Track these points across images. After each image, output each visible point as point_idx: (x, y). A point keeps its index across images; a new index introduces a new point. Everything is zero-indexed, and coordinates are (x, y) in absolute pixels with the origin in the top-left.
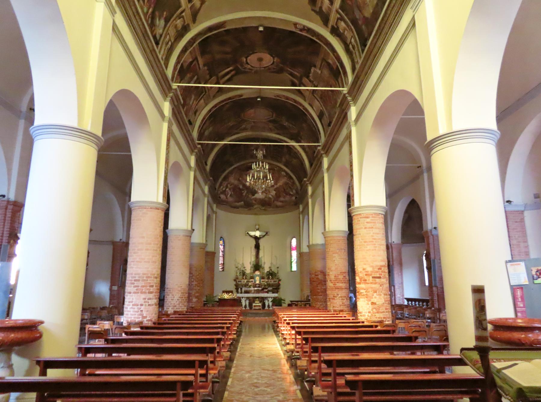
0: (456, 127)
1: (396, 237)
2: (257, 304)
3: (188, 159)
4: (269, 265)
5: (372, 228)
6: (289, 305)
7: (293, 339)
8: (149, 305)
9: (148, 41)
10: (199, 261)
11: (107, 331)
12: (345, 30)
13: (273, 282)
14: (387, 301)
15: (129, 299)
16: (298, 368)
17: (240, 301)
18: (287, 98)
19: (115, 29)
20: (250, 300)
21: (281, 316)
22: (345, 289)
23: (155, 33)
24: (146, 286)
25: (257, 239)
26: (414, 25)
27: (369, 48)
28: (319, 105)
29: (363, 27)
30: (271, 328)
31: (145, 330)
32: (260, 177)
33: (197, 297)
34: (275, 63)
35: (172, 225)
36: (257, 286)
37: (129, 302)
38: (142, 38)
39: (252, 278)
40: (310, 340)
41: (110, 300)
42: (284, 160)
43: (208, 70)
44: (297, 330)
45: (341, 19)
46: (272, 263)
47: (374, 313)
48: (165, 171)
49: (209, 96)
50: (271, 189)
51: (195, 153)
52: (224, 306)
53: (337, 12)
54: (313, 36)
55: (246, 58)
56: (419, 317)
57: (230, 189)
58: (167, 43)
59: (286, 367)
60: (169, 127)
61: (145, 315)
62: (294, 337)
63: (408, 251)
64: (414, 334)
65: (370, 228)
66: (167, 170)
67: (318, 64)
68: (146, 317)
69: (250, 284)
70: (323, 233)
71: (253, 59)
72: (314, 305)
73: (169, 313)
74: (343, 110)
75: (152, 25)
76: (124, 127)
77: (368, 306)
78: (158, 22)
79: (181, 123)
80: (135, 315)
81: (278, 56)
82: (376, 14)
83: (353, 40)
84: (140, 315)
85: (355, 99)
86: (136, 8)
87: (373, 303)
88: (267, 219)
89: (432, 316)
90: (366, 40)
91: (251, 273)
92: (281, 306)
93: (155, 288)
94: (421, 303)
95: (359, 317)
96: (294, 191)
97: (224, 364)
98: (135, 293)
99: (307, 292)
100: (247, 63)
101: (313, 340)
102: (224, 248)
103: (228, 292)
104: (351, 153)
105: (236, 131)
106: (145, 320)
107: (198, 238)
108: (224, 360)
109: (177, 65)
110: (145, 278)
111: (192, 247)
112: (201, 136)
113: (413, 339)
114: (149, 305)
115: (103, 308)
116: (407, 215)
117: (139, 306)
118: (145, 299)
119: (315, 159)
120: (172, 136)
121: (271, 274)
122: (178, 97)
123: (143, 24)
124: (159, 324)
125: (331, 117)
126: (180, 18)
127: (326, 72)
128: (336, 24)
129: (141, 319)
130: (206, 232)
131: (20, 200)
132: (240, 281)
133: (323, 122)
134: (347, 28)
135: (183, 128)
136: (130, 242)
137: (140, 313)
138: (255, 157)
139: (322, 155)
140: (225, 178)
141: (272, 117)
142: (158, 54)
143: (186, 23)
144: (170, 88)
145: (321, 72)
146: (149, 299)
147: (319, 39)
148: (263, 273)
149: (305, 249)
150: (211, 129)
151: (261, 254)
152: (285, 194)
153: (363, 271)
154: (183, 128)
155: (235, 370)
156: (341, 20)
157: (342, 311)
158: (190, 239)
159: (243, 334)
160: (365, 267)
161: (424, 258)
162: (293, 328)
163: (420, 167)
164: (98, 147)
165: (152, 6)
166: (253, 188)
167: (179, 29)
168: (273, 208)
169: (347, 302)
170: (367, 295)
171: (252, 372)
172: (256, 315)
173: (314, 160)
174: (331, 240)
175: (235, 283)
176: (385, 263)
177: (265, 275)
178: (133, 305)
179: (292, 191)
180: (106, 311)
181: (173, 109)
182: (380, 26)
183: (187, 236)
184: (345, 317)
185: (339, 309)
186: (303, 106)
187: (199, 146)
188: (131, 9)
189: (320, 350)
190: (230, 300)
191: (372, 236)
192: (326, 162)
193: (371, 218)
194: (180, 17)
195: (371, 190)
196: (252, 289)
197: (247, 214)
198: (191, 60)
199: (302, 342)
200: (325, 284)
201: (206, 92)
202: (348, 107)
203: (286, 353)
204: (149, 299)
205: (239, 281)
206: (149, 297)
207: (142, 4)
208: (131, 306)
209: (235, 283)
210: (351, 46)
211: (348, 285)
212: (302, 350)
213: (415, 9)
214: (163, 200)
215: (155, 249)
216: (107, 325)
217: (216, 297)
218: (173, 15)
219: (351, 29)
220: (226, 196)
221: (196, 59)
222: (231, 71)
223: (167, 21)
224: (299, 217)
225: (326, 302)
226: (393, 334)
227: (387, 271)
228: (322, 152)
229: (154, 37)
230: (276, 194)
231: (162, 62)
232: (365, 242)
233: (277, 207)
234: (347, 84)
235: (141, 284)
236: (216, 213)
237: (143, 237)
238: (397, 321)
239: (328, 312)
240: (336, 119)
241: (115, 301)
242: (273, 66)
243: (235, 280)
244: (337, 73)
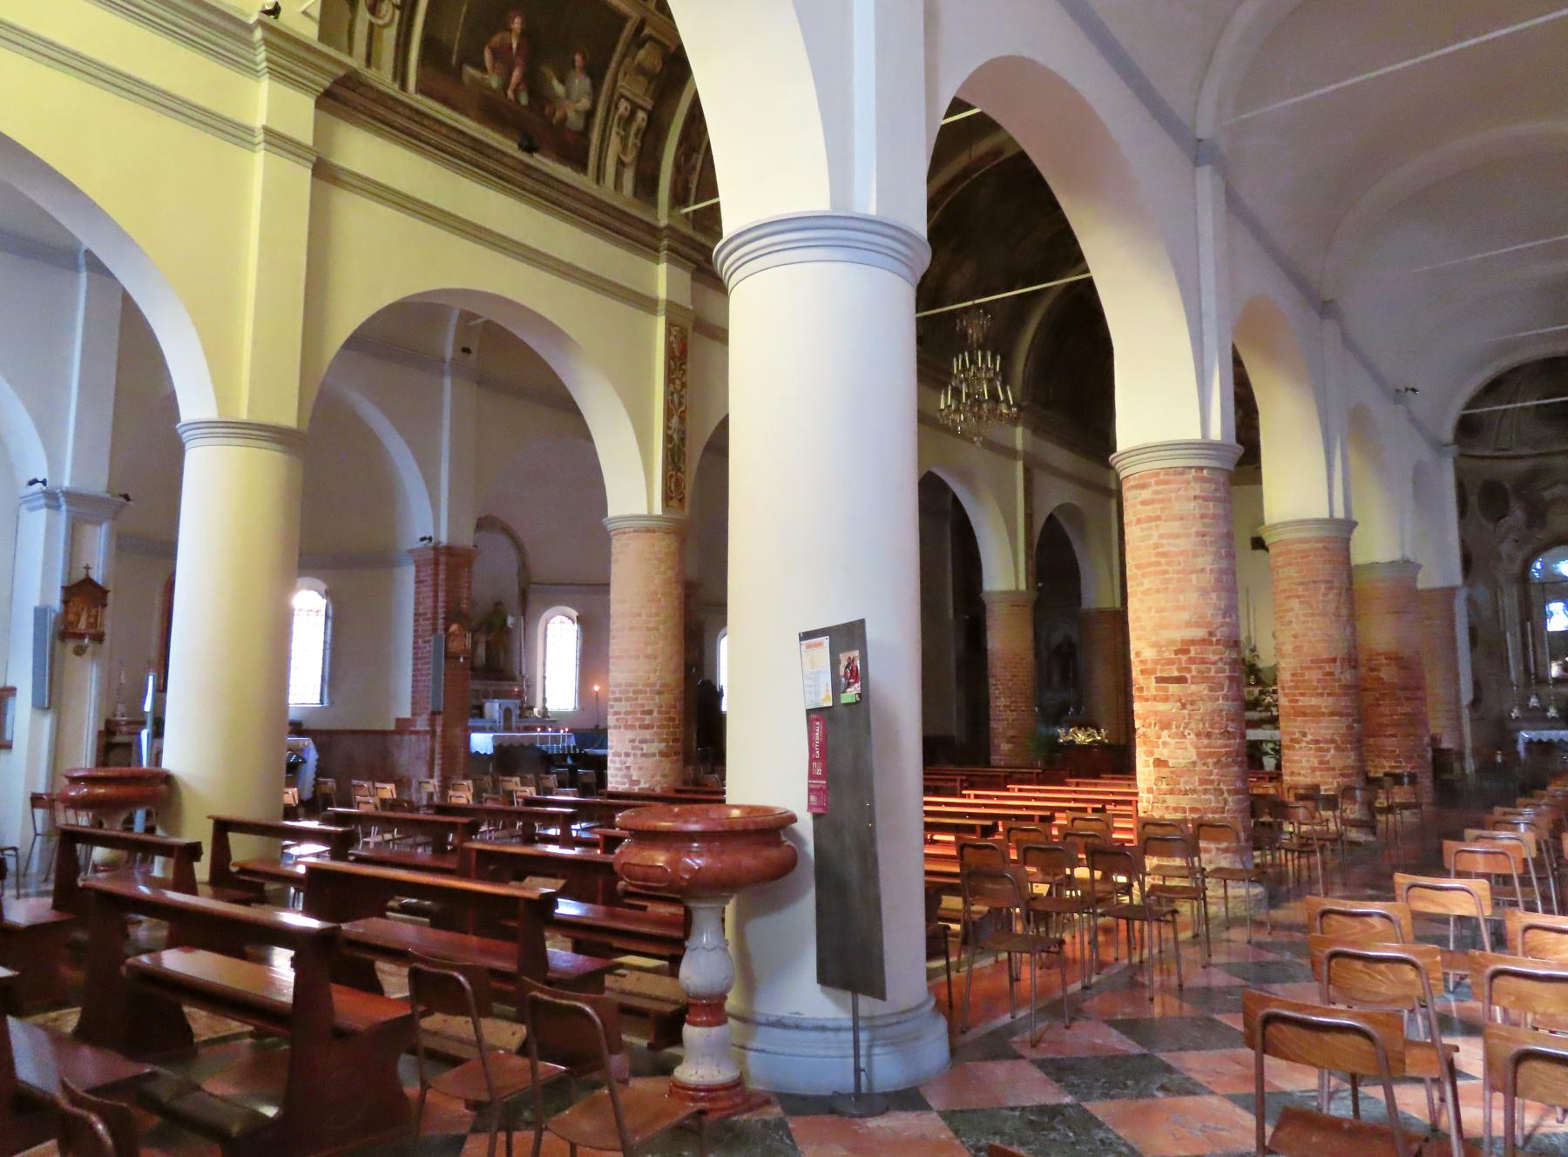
5: (1158, 518)
58: (628, 121)
65: (1150, 519)
68: (638, 782)
76: (1076, 259)
84: (625, 776)
114: (643, 755)
118: (633, 741)
126: (641, 46)
144: (653, 230)
146: (642, 742)
191: (1156, 546)
204: (643, 741)
223: (596, 74)
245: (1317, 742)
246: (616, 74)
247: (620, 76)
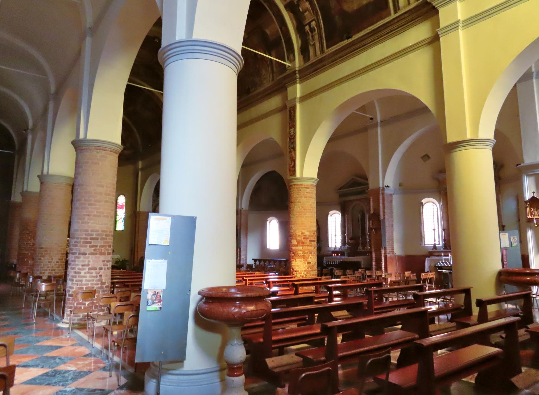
1: (245, 205)
11: (277, 292)
29: (337, 18)
61: (104, 281)
77: (305, 265)
80: (93, 280)
83: (313, 24)
87: (308, 263)
98: (92, 254)
106: (104, 286)
110: (104, 236)
117: (98, 270)
118: (104, 261)
137: (98, 278)
160: (303, 231)
183: (70, 185)
191: (311, 205)
219: (317, 12)
235: (99, 243)
237: (102, 186)
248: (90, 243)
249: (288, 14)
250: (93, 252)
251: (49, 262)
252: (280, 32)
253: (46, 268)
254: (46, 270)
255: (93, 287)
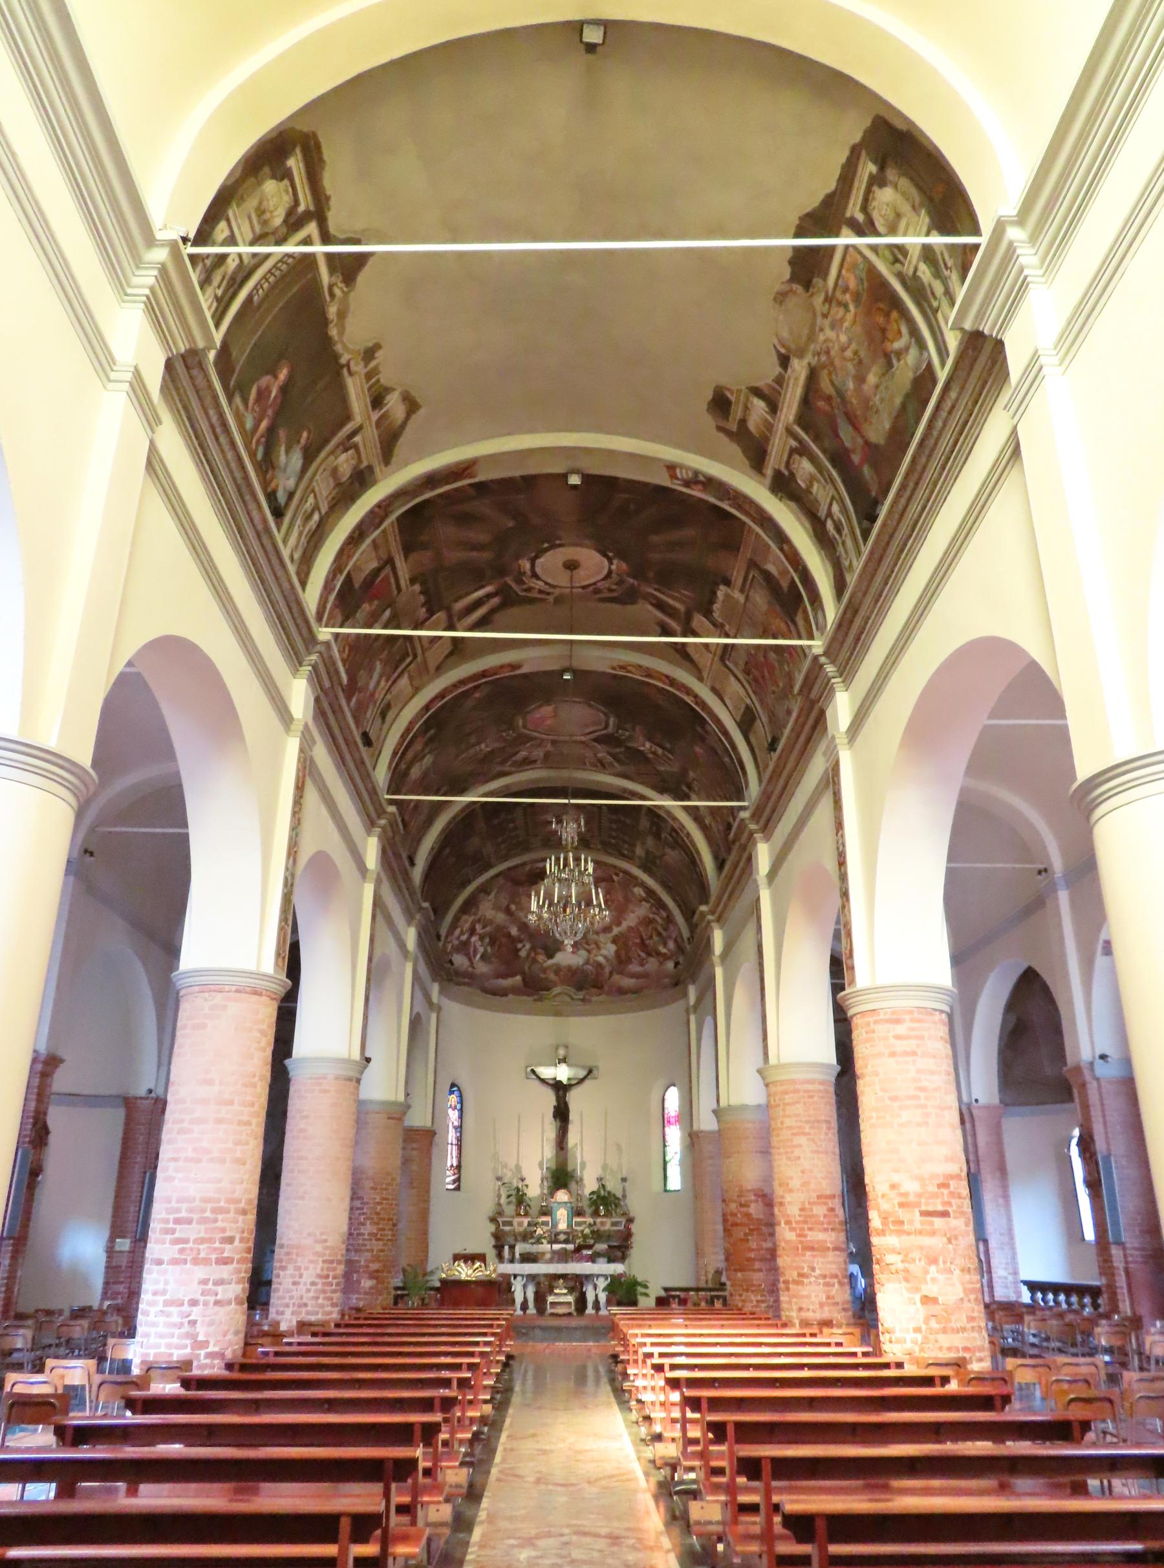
0: (880, 982)
1: (984, 1085)
2: (562, 1297)
3: (359, 845)
4: (599, 1172)
5: (914, 1053)
6: (662, 1302)
7: (674, 1421)
8: (217, 1303)
9: (252, 506)
10: (381, 1157)
11: (70, 1396)
12: (812, 479)
13: (609, 1227)
14: (973, 1291)
15: (156, 1282)
16: (695, 1528)
17: (510, 1285)
18: (649, 673)
19: (154, 464)
20: (538, 1284)
21: (633, 1341)
22: (836, 1249)
23: (273, 485)
24: (211, 1240)
25: (560, 1089)
26: (1018, 446)
27: (884, 525)
28: (741, 691)
30: (604, 1380)
31: (199, 1390)
32: (569, 898)
33: (373, 1275)
34: (614, 575)
35: (304, 1043)
36: (562, 1237)
37: (155, 1293)
38: (234, 496)
39: (546, 1212)
40: (730, 1430)
41: (107, 1283)
42: (639, 851)
43: (421, 593)
44: (689, 1393)
45: (802, 450)
46: (605, 1167)
47: (931, 1331)
48: (286, 879)
49: (427, 668)
50: (602, 938)
51: (306, 669)
52: (456, 1304)
53: (789, 432)
54: (721, 500)
55: (533, 561)
56: (1074, 1345)
57: (482, 938)
58: (308, 517)
59: (654, 1519)
60: (301, 750)
61: (201, 1338)
62: (676, 1414)
63: (1023, 1132)
64: (1076, 1413)
66: (293, 875)
67: (737, 577)
68: (205, 1344)
69: (539, 1231)
70: (759, 1071)
71: (550, 564)
72: (737, 1301)
73: (283, 1327)
74: (813, 703)
75: (267, 465)
78: (283, 458)
79: (341, 740)
80: (172, 1336)
81: (622, 555)
82: (899, 436)
83: (835, 508)
84: (187, 1335)
85: (847, 671)
86: (221, 415)
87: (927, 1300)
88: (591, 1030)
89: (1117, 1342)
90: (876, 503)
91: (542, 1197)
92: (634, 1303)
93: (240, 1249)
94: (1074, 1299)
95: (886, 1347)
96: (671, 945)
97: (445, 1512)
98: (174, 1262)
99: (715, 1259)
100: (535, 575)
101: (746, 1430)
102: (461, 1117)
103: (469, 1258)
104: (839, 825)
105: (499, 768)
106: (202, 1353)
107: (382, 1085)
108: (447, 1500)
109: (335, 576)
110: (208, 1214)
111: (361, 1113)
112: (398, 781)
113: (998, 1403)
114: (217, 1303)
115: (80, 1313)
116: (1013, 1019)
118: (205, 1282)
119: (733, 847)
120: (315, 781)
121: (604, 1201)
122: (334, 663)
123: (240, 459)
124: (243, 1367)
125: (776, 725)
126: (346, 450)
127: (760, 599)
128: (788, 464)
129: (188, 1350)
130: (408, 1066)
131: (160, 1091)
132: (510, 1224)
133: (753, 740)
134: (818, 475)
135: (348, 757)
136: (169, 1098)
138: (553, 843)
139: (751, 834)
140: (469, 906)
141: (606, 727)
142: (281, 545)
143: (365, 464)
144: (311, 640)
145: (747, 598)
146: (216, 1283)
147: (739, 508)
148: (579, 1197)
149: (706, 1122)
150: (428, 760)
151: (572, 1138)
152: (643, 955)
153: (892, 1194)
154: (348, 757)
155: (483, 1535)
156: (801, 455)
157: (828, 1323)
158: (357, 1089)
159: (516, 1399)
160: (896, 1178)
161: (1074, 1151)
162: (674, 1384)
163: (1046, 870)
164: (78, 800)
165: (270, 412)
166: (547, 932)
167: (344, 479)
168: (609, 993)
169: (843, 1295)
170: (906, 1271)
171: (541, 1543)
172: (558, 1333)
173: (729, 850)
174: (786, 1092)
175: (492, 1228)
176: (958, 1166)
177: (585, 1204)
178: (167, 1303)
179: (665, 945)
180: (85, 1323)
181: (317, 700)
182: (914, 460)
183: (350, 1079)
184: (839, 1344)
185: (819, 1316)
186: (696, 696)
187: (392, 809)
188: (207, 414)
189: (767, 1469)
190: (478, 1283)
192: (763, 855)
193: (908, 1024)
194: (347, 445)
195: (905, 938)
196: (545, 1247)
197: (529, 1013)
198: (374, 564)
199: (705, 1435)
200: (772, 1235)
201: (415, 656)
202: (828, 692)
203: (653, 1471)
204: (219, 1282)
205: (505, 1223)
206: (217, 1276)
207: (241, 407)
208: (160, 1307)
209: (492, 1228)
210: (830, 525)
211: (842, 1237)
212: (707, 1464)
213: (1019, 408)
214: (276, 964)
215: (245, 1118)
216: (79, 1372)
217: (432, 1273)
218: (327, 441)
219: (830, 476)
220: (470, 959)
221: (390, 561)
222: (489, 596)
223: (309, 456)
224: (688, 1020)
225: (774, 1290)
226: (943, 1385)
227: (965, 1192)
228: (753, 827)
229: (271, 496)
230: (617, 953)
231: (292, 569)
232: (894, 1099)
233: (621, 991)
234: (822, 628)
235: (193, 1232)
236: (439, 1009)
237: (210, 1082)
238: (1011, 1363)
239: (785, 1325)
240: (792, 730)
241: (121, 1288)
242: (606, 584)
243: (493, 1220)
244: (791, 600)
245: (824, 1277)
246: (317, 470)
247: (320, 471)
248: (173, 1231)
249: (786, 505)
250: (177, 1256)
251: (295, 1283)
252: (784, 560)
253: (287, 1300)
254: (287, 1306)
255: (171, 1355)
